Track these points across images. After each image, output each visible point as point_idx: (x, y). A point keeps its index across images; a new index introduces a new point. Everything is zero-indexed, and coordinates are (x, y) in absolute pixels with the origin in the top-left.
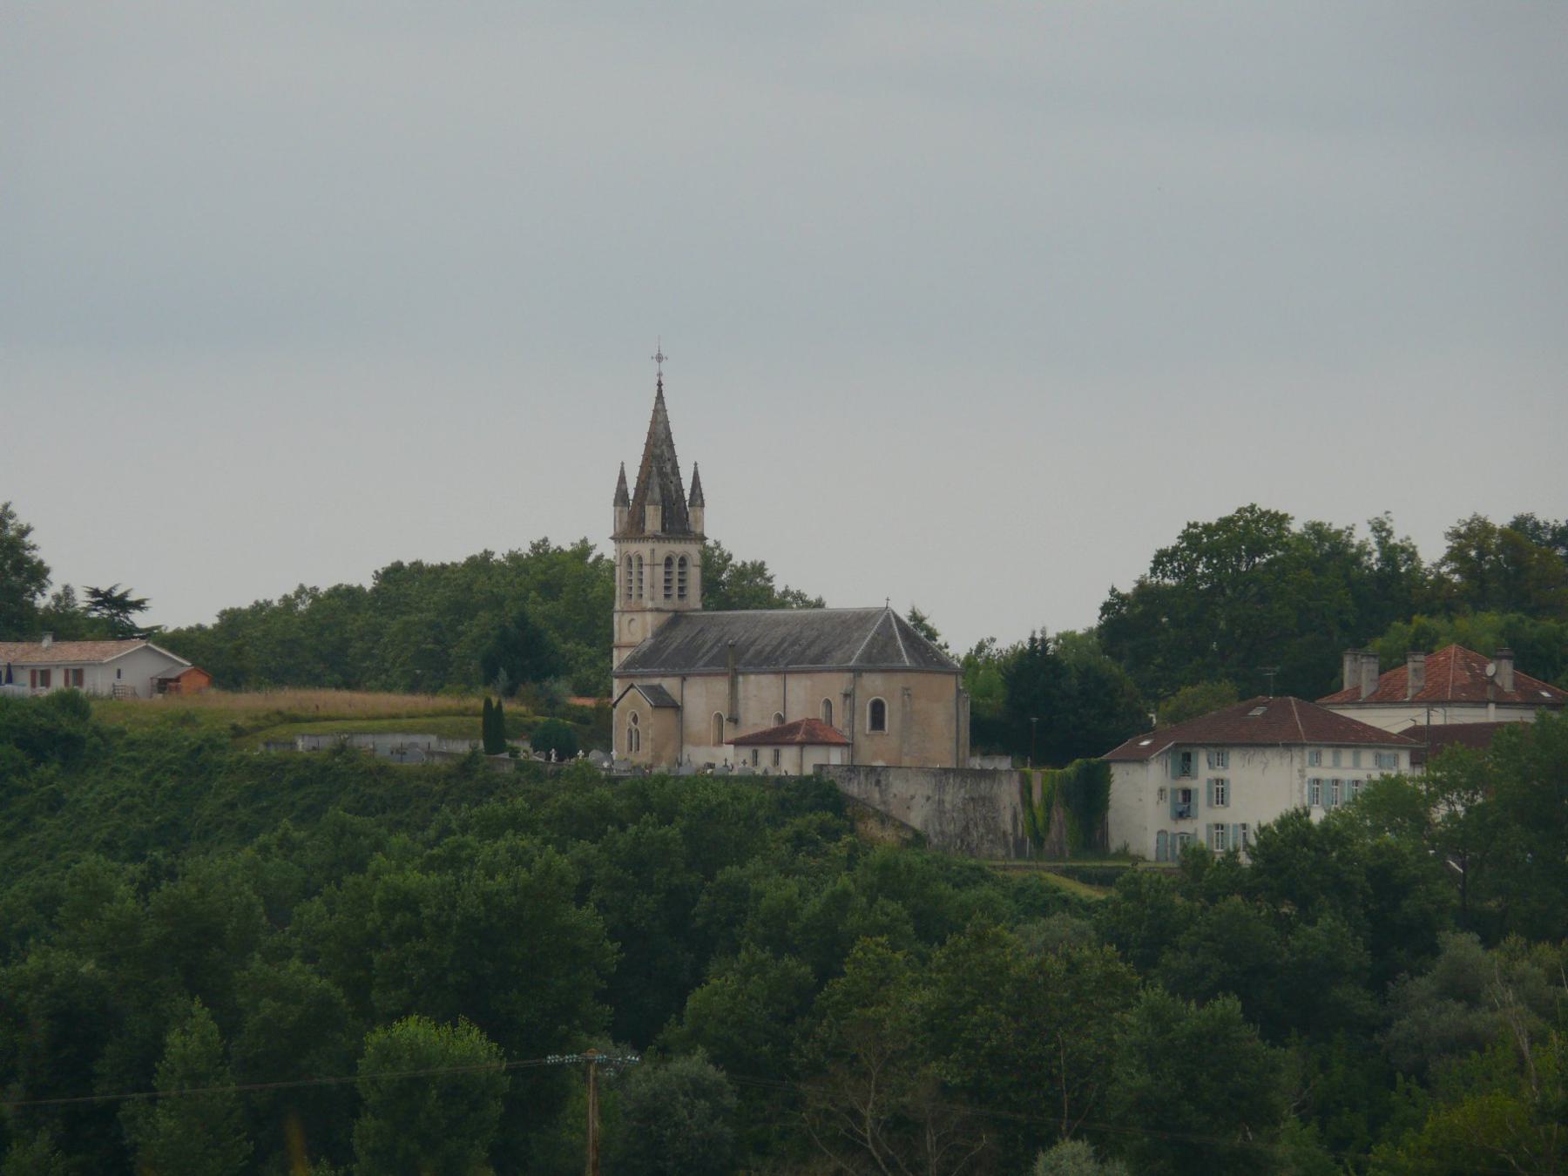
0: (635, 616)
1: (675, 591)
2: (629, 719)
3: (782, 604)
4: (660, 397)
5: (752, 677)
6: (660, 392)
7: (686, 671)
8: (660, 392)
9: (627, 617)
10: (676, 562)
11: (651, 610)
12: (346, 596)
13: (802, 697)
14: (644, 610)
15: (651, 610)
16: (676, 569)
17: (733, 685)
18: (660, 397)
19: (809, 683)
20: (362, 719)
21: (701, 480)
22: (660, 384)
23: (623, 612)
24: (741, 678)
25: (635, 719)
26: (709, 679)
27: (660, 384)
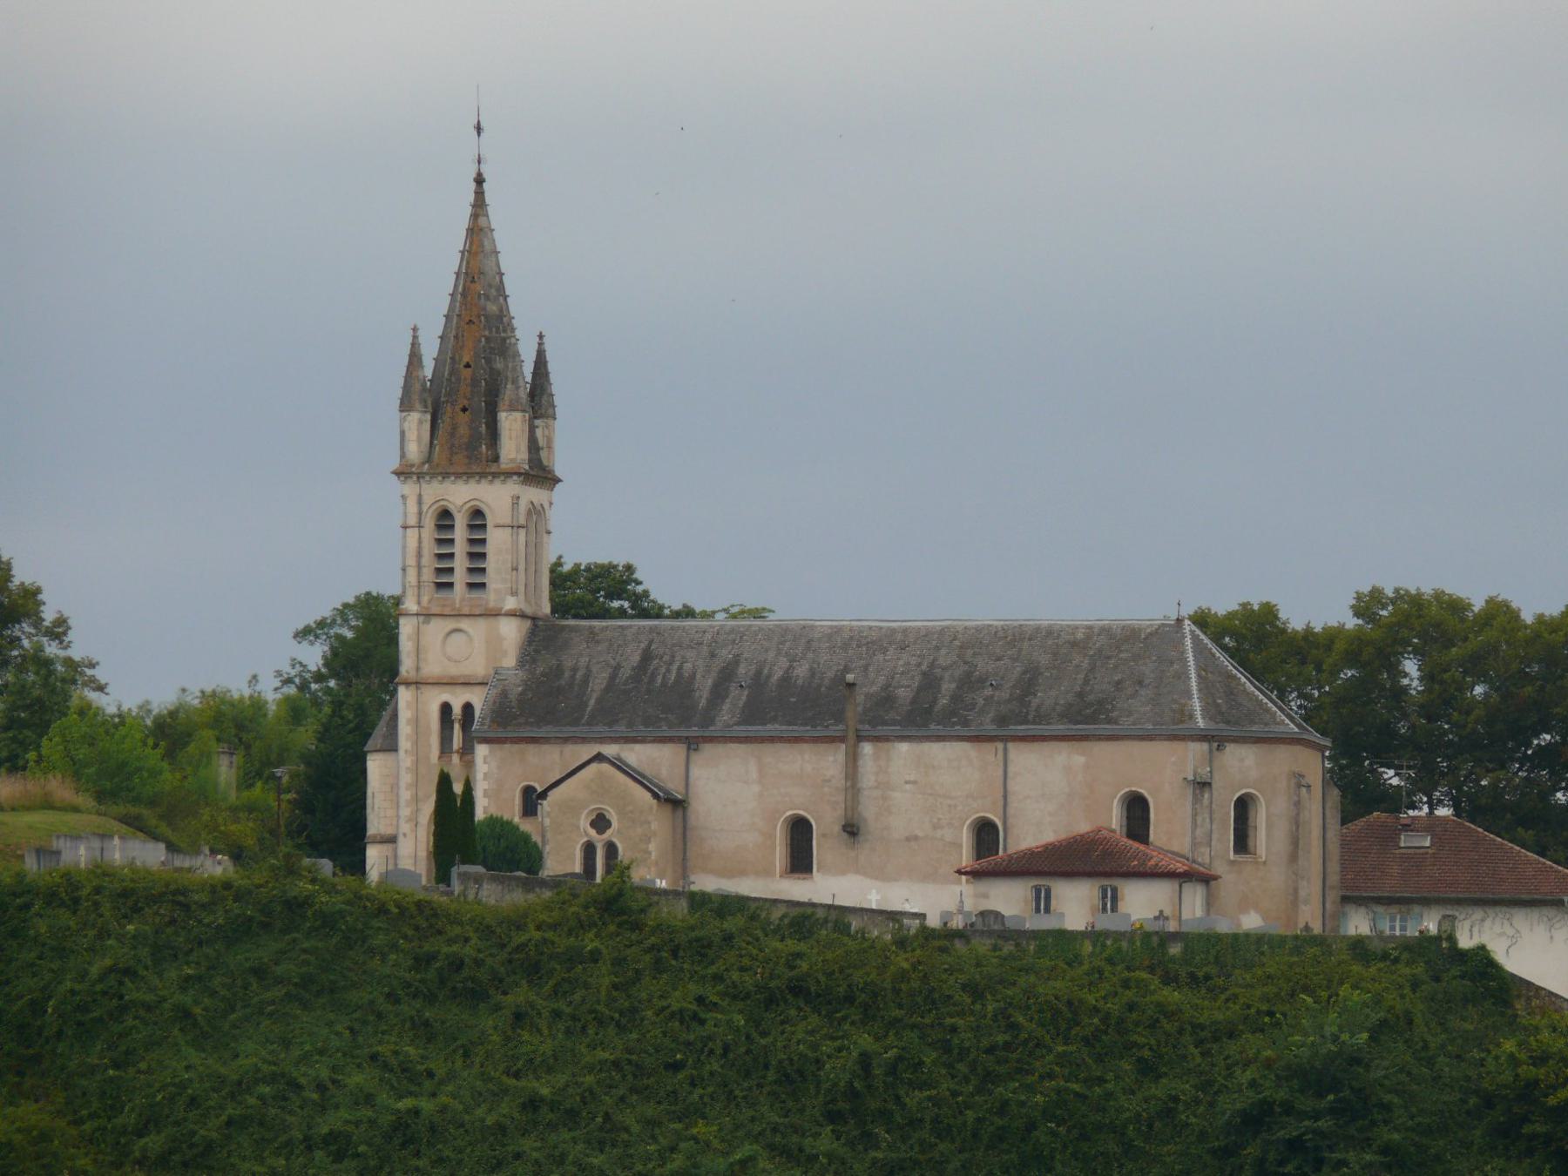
0: (464, 624)
1: (460, 577)
2: (584, 822)
3: (659, 616)
4: (480, 204)
5: (904, 747)
6: (479, 194)
7: (694, 731)
8: (479, 194)
9: (437, 628)
10: (460, 522)
11: (512, 614)
12: (1456, 607)
13: (1051, 790)
14: (495, 614)
15: (512, 614)
16: (460, 533)
17: (853, 759)
18: (480, 204)
19: (1079, 760)
20: (29, 809)
21: (551, 367)
22: (479, 180)
23: (427, 616)
24: (867, 748)
25: (601, 823)
26: (767, 748)
27: (479, 180)
